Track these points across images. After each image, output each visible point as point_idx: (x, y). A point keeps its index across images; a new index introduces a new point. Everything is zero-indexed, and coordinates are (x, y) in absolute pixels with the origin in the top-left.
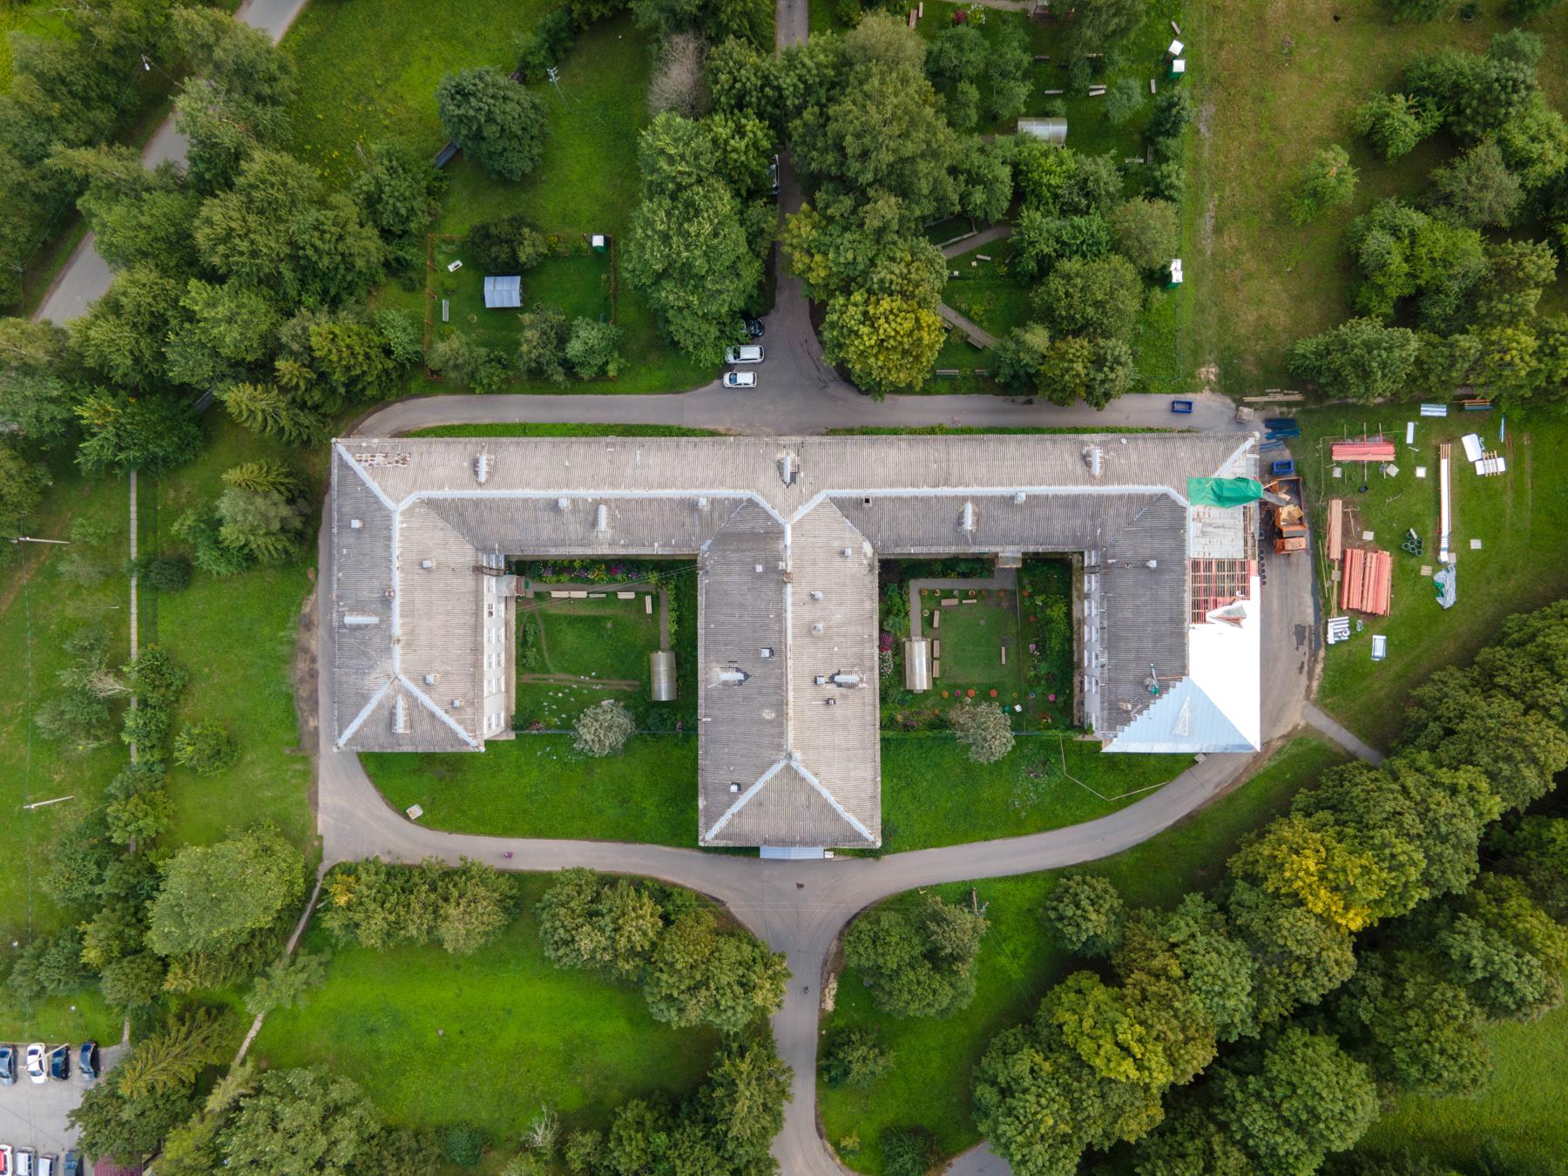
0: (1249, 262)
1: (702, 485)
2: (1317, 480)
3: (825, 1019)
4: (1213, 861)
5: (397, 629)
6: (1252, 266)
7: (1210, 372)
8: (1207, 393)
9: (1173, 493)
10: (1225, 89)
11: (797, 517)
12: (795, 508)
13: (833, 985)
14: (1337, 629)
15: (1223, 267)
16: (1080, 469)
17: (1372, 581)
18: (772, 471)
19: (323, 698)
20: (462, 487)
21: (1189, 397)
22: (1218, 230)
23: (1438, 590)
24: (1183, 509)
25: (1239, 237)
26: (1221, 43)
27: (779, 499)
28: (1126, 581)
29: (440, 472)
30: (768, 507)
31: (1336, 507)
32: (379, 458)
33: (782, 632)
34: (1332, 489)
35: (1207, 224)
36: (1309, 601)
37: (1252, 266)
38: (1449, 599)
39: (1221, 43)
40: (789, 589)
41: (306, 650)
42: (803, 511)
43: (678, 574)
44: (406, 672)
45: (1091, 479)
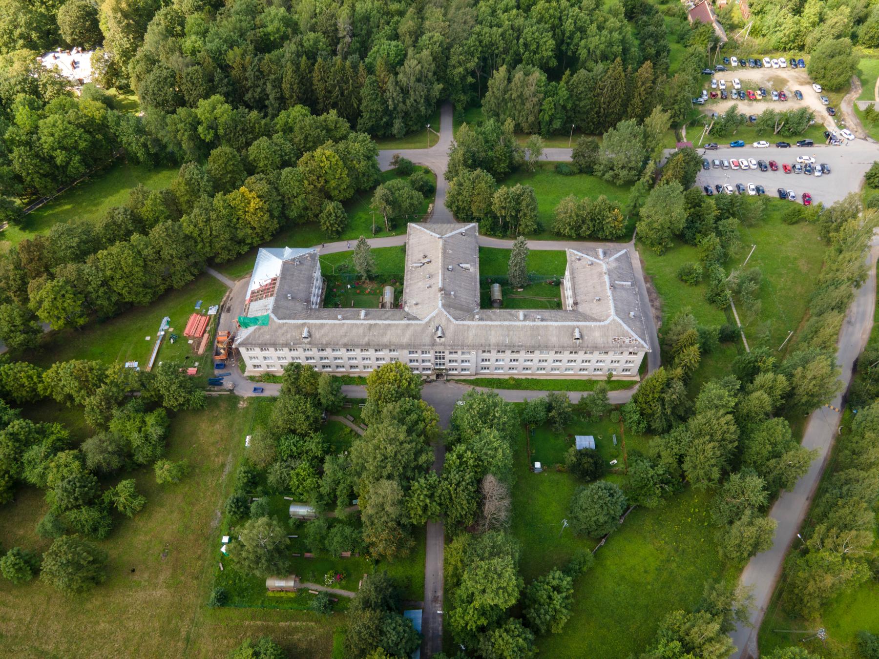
0: (213, 451)
1: (478, 326)
2: (206, 362)
3: (433, 202)
4: (284, 230)
5: (606, 278)
6: (211, 449)
7: (242, 405)
8: (246, 396)
9: (275, 319)
10: (203, 533)
11: (436, 311)
12: (437, 315)
13: (429, 210)
14: (213, 311)
15: (225, 449)
16: (313, 331)
17: (194, 325)
18: (447, 333)
19: (645, 293)
20: (586, 327)
21: (254, 395)
22: (223, 465)
23: (168, 323)
24: (273, 312)
25: (214, 461)
26: (199, 558)
27: (444, 319)
28: (302, 295)
29: (597, 334)
30: (449, 316)
31: (201, 351)
32: (627, 341)
33: (443, 274)
34: (200, 358)
35: (228, 468)
36: (222, 321)
37: (211, 449)
38: (166, 319)
39: (199, 558)
40: (440, 285)
41: (656, 309)
42: (433, 314)
43: (487, 302)
44: (601, 265)
45: (309, 326)
